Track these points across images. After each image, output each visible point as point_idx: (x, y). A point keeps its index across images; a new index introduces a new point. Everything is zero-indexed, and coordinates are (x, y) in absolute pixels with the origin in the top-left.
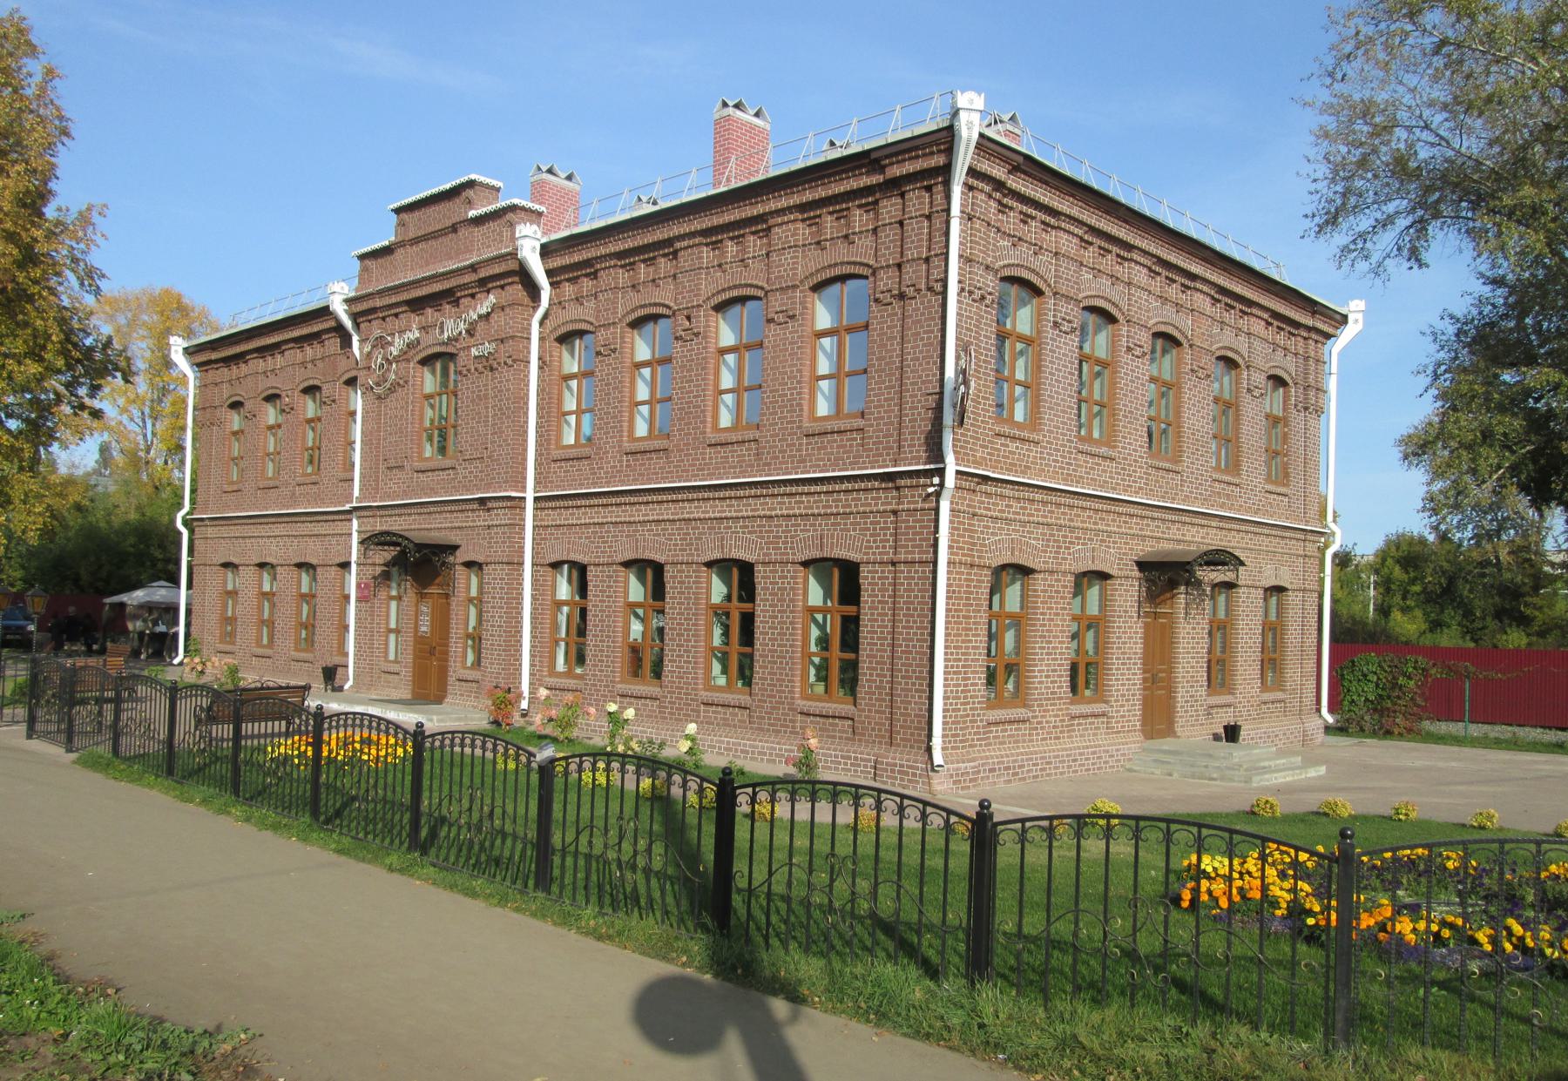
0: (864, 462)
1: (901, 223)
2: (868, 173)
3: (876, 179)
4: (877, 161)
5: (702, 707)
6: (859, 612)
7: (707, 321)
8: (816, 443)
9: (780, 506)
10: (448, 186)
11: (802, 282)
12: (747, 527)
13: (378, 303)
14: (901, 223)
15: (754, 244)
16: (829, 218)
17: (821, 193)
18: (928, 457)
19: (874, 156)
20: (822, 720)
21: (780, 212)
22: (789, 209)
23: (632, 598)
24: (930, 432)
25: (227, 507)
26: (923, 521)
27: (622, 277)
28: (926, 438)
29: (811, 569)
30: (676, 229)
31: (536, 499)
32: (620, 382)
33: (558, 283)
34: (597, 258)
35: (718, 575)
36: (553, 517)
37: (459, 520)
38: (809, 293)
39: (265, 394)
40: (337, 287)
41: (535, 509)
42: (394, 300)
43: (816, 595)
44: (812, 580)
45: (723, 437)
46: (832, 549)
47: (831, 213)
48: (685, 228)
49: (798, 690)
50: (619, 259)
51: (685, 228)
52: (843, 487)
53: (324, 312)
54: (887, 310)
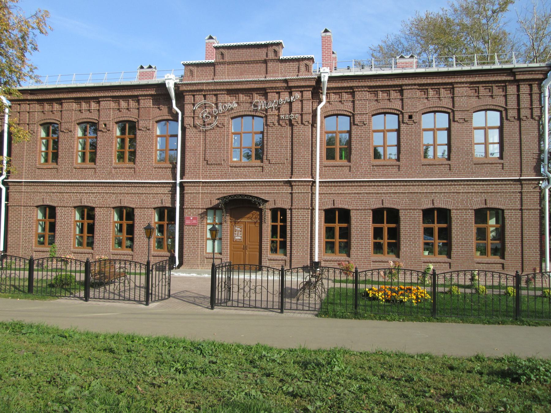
0: (360, 177)
1: (99, 110)
2: (506, 76)
3: (509, 78)
4: (514, 72)
5: (34, 253)
6: (55, 221)
7: (38, 129)
8: (479, 167)
9: (461, 189)
10: (263, 43)
11: (37, 122)
12: (445, 196)
13: (204, 88)
14: (99, 110)
15: (56, 106)
16: (482, 88)
17: (429, 81)
18: (536, 174)
19: (514, 70)
20: (486, 265)
21: (460, 83)
22: (466, 83)
23: (39, 218)
24: (535, 166)
25: (45, 177)
26: (534, 195)
27: (113, 105)
28: (534, 168)
29: (39, 208)
30: (406, 81)
31: (320, 182)
32: (28, 145)
33: (329, 93)
34: (356, 86)
35: (40, 211)
36: (326, 190)
37: (267, 189)
38: (39, 126)
39: (42, 122)
40: (172, 76)
41: (320, 186)
42: (222, 87)
43: (40, 216)
44: (76, 212)
45: (235, 164)
46: (495, 204)
47: (483, 87)
48: (145, 93)
49: (72, 245)
50: (369, 88)
51: (145, 93)
52: (459, 183)
53: (162, 86)
54: (512, 123)
